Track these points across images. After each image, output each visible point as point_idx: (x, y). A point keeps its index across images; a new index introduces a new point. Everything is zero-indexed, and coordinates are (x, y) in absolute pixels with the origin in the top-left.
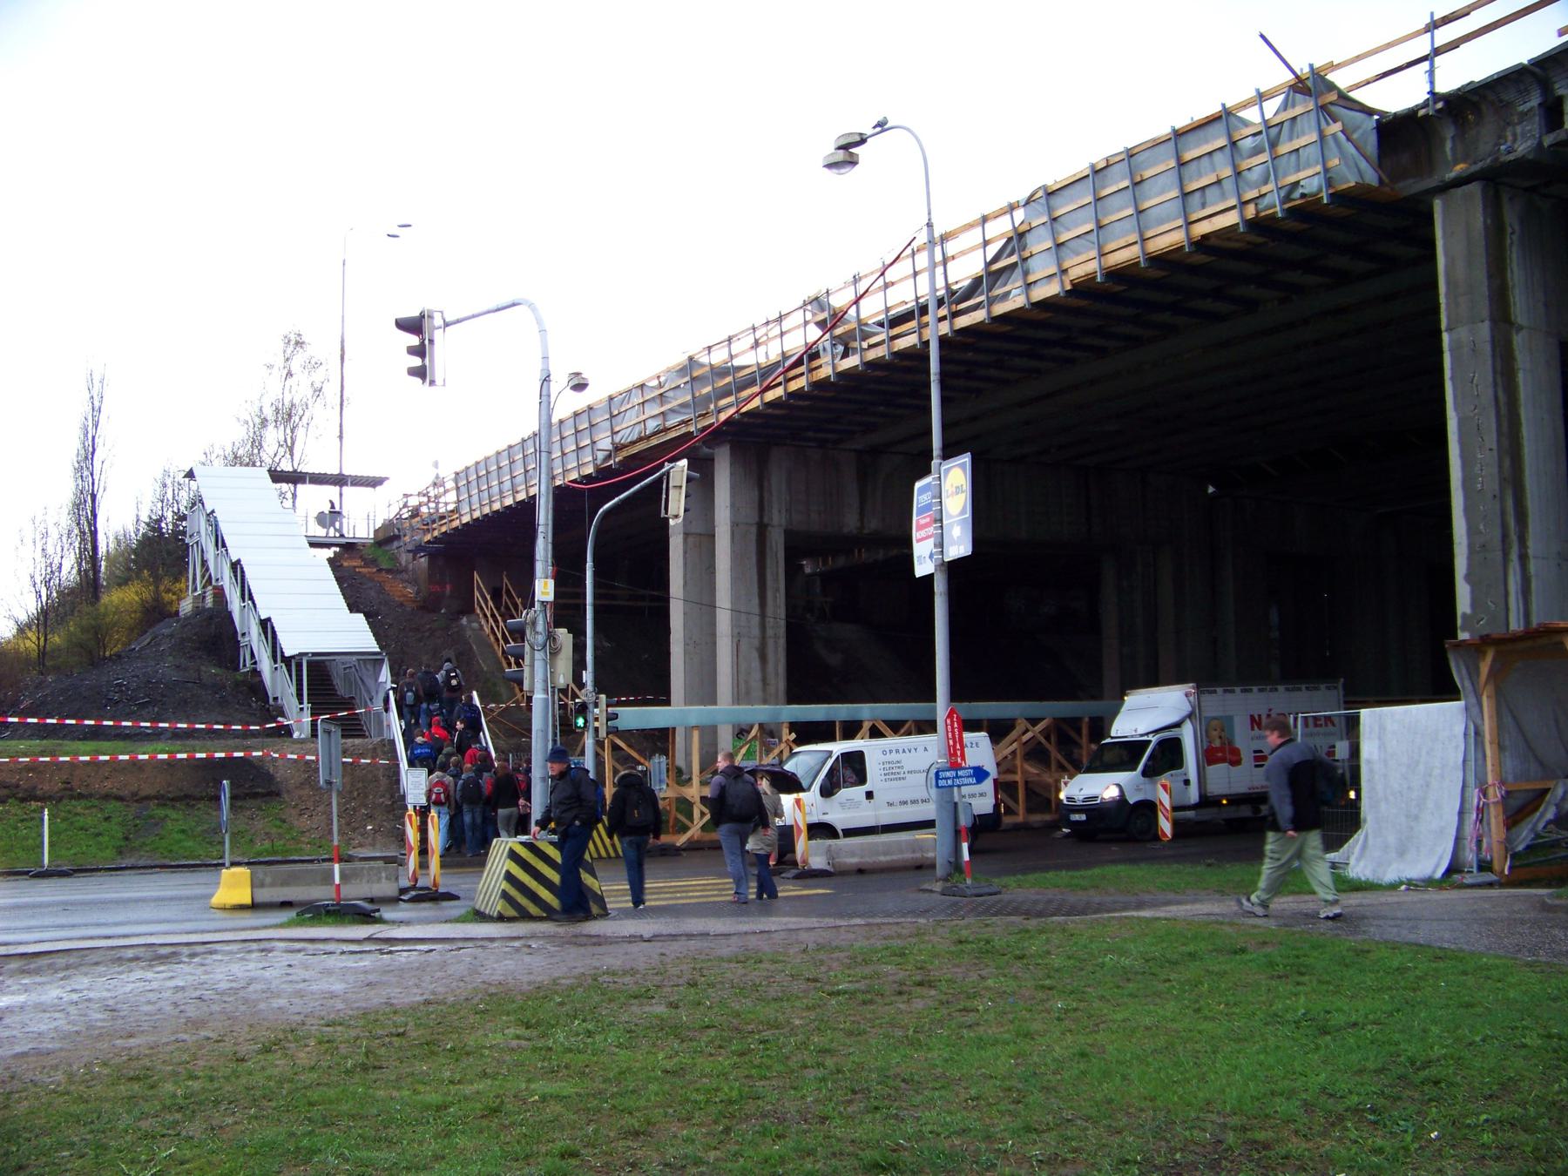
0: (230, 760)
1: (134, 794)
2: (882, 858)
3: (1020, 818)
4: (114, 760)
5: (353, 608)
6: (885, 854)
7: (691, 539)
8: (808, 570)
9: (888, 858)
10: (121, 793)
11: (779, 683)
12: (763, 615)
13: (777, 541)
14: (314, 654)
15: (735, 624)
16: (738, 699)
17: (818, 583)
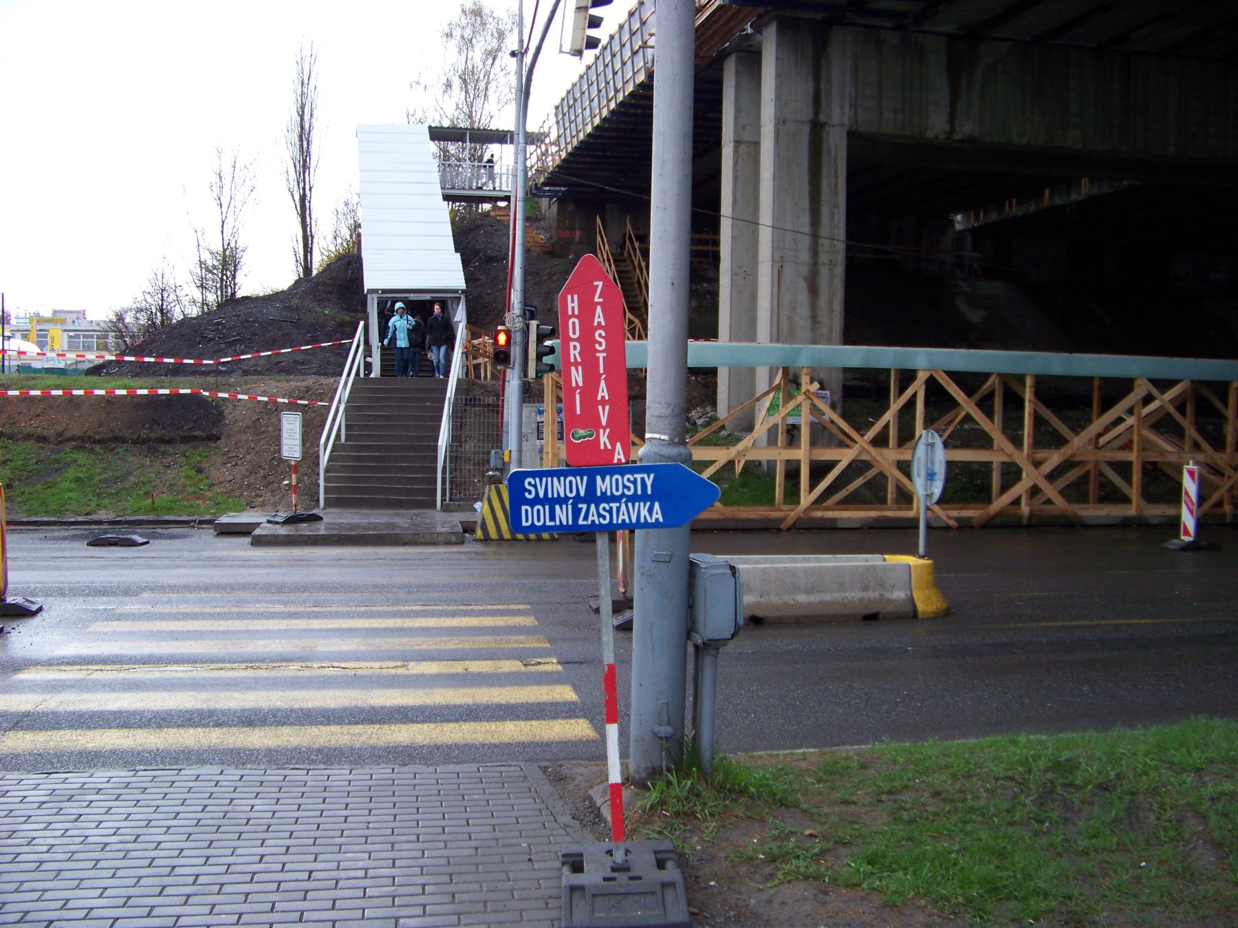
0: (175, 398)
1: (60, 434)
2: (802, 598)
3: (1131, 511)
4: (46, 396)
5: (456, 251)
6: (810, 590)
7: (743, 148)
8: (958, 227)
9: (814, 598)
10: (45, 433)
11: (834, 318)
12: (815, 235)
13: (837, 145)
14: (384, 291)
15: (776, 246)
16: (777, 337)
17: (969, 240)
